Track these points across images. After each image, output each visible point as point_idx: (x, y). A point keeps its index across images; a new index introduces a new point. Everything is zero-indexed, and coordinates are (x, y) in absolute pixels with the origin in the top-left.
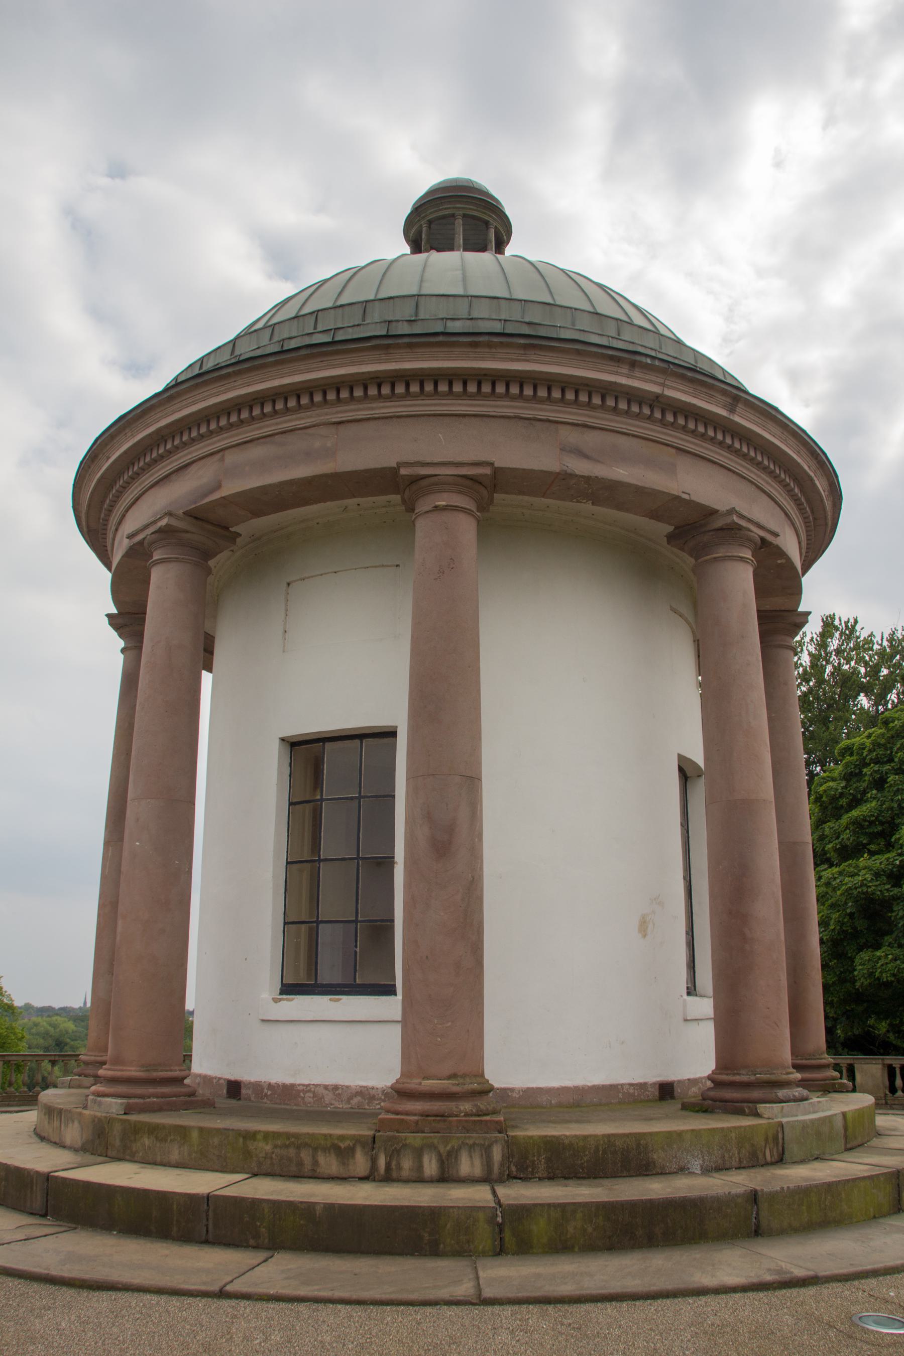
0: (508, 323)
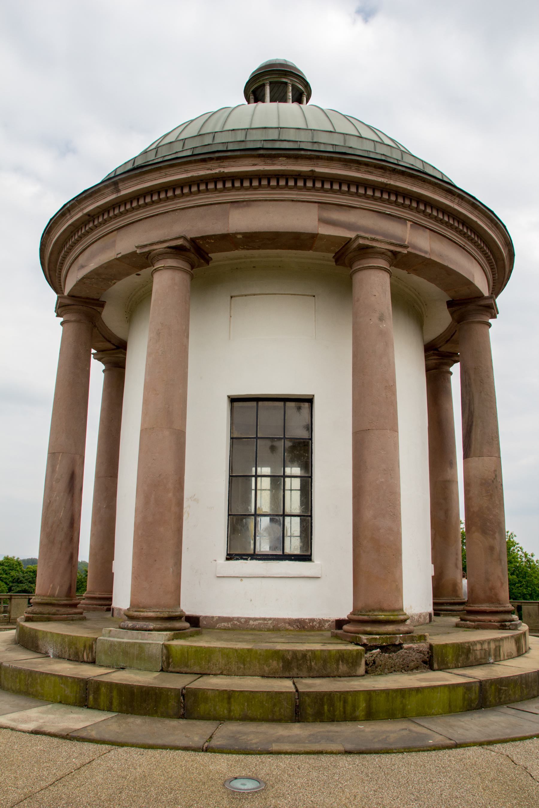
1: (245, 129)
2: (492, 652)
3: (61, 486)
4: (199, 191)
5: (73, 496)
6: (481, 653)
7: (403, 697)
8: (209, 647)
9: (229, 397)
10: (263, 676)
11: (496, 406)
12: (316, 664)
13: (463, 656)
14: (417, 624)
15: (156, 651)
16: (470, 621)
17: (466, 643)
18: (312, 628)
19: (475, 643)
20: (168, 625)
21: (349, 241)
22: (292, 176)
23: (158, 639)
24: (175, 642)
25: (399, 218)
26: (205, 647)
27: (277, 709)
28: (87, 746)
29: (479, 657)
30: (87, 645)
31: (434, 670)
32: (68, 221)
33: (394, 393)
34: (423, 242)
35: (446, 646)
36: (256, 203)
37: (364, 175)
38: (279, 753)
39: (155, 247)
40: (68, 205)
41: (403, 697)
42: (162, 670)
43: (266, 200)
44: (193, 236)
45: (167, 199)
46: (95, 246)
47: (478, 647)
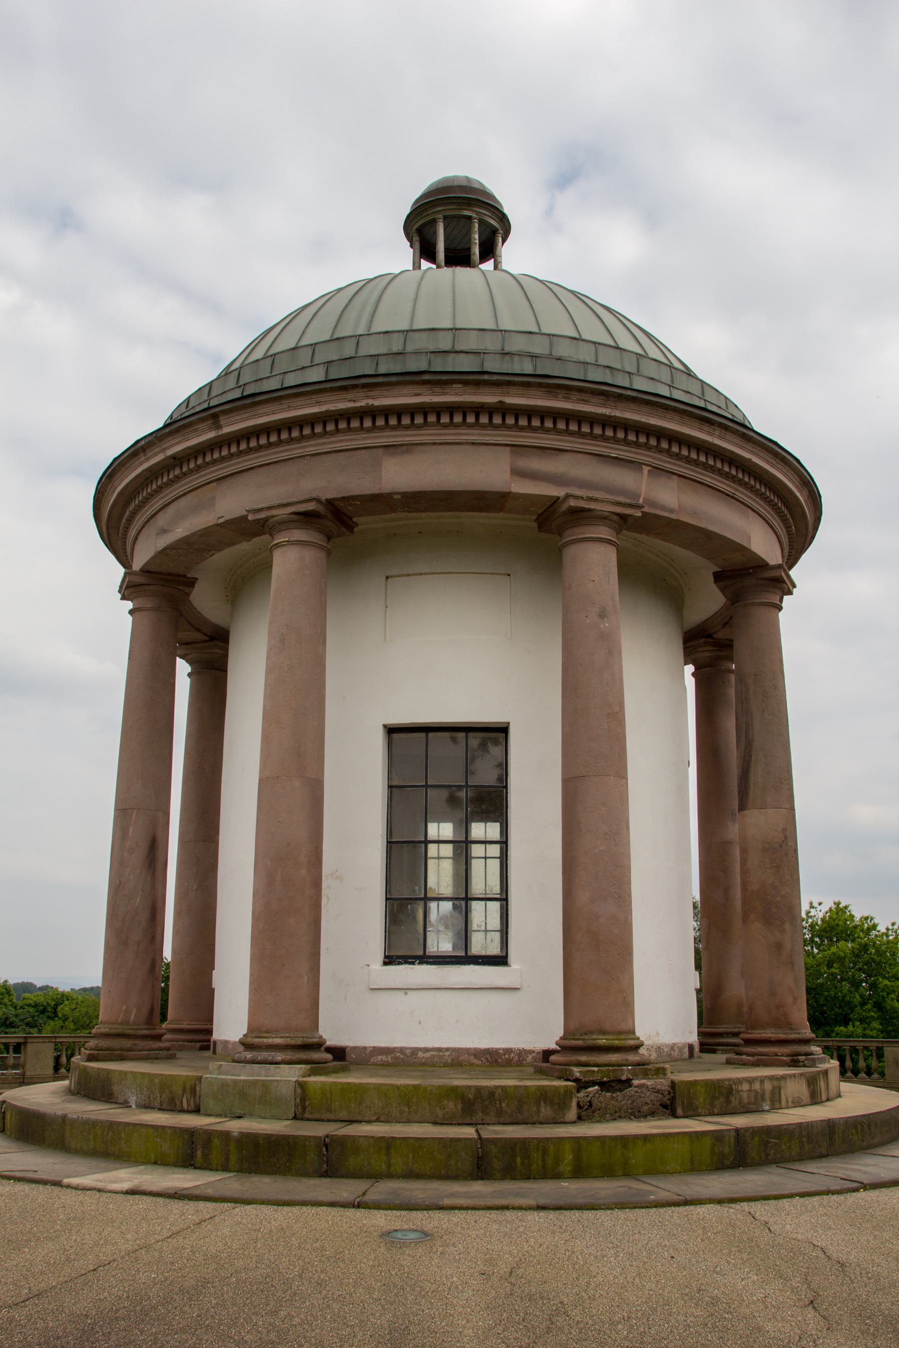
1: (403, 331)
2: (767, 1095)
3: (138, 857)
4: (337, 430)
5: (154, 874)
6: (749, 1096)
7: (625, 1147)
8: (361, 1084)
9: (385, 726)
10: (435, 1123)
11: (788, 731)
12: (508, 1105)
13: (722, 1099)
14: (668, 1059)
15: (287, 1091)
16: (748, 1054)
17: (725, 1080)
18: (509, 1063)
19: (740, 1081)
20: (303, 1055)
21: (555, 501)
22: (471, 408)
23: (289, 1075)
24: (313, 1079)
25: (631, 462)
26: (354, 1084)
27: (452, 1162)
28: (202, 1205)
29: (746, 1101)
30: (188, 1086)
31: (677, 1117)
32: (141, 463)
33: (621, 723)
34: (668, 496)
35: (694, 1083)
36: (420, 447)
37: (575, 405)
38: (452, 1208)
39: (275, 512)
40: (143, 443)
41: (625, 1147)
42: (295, 1118)
43: (435, 444)
44: (330, 495)
45: (291, 440)
46: (183, 502)
47: (745, 1086)
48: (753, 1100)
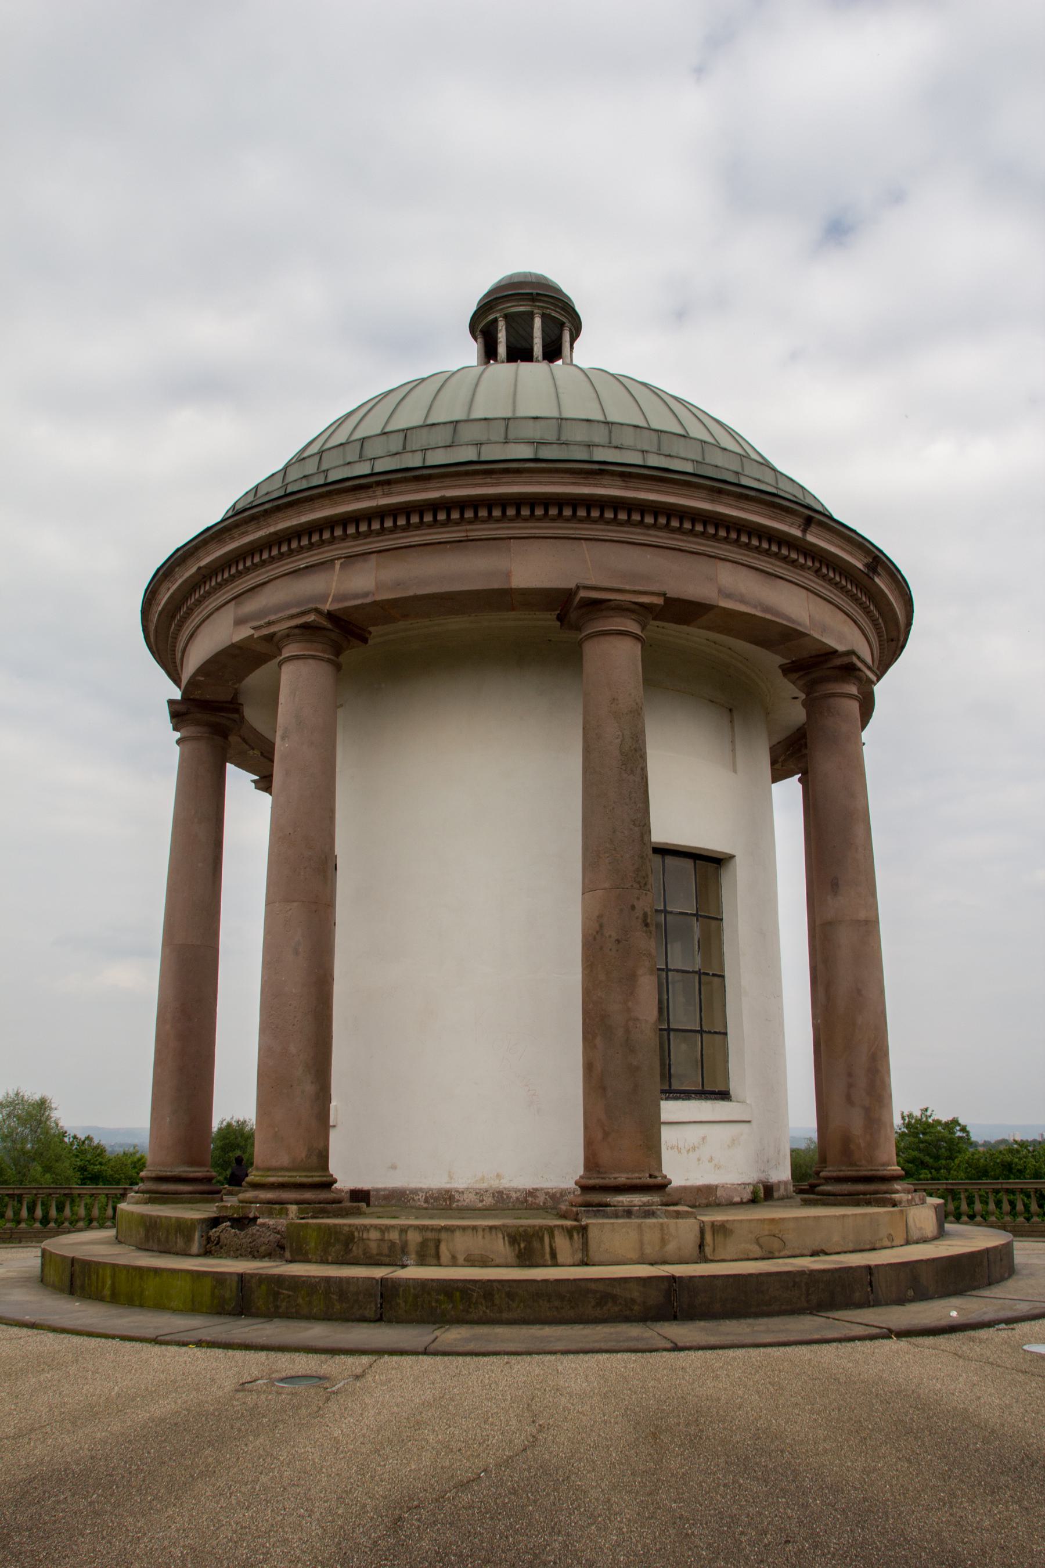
0: (429, 453)
25: (322, 563)
41: (141, 1278)
48: (386, 1251)
